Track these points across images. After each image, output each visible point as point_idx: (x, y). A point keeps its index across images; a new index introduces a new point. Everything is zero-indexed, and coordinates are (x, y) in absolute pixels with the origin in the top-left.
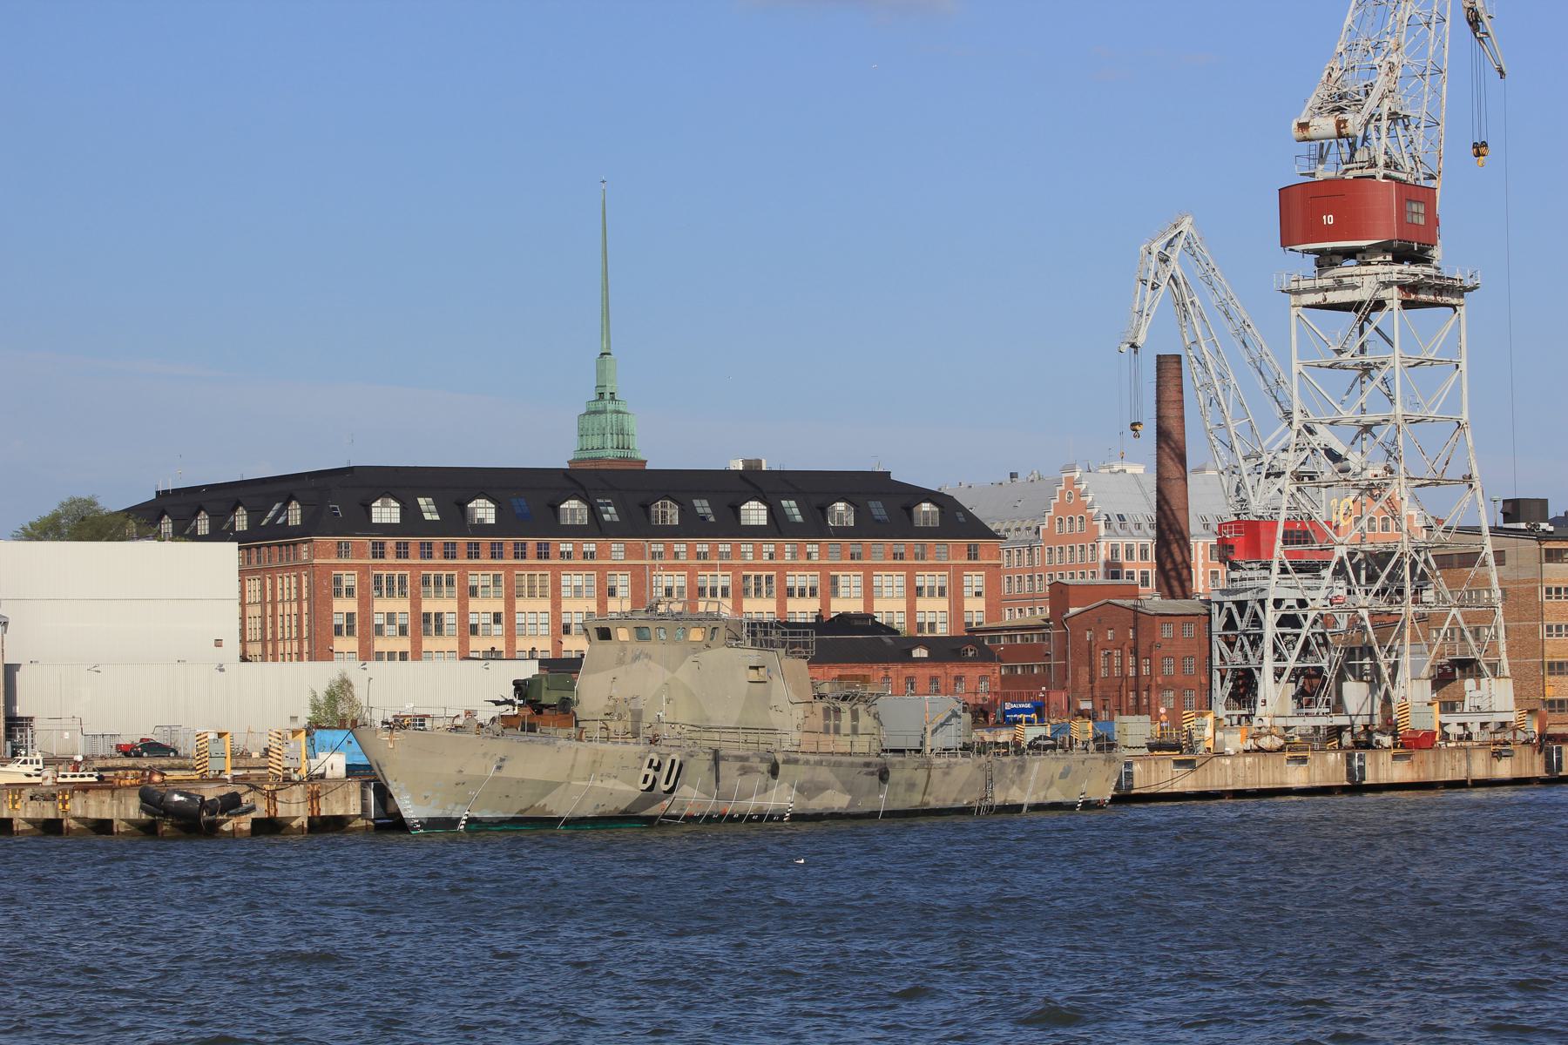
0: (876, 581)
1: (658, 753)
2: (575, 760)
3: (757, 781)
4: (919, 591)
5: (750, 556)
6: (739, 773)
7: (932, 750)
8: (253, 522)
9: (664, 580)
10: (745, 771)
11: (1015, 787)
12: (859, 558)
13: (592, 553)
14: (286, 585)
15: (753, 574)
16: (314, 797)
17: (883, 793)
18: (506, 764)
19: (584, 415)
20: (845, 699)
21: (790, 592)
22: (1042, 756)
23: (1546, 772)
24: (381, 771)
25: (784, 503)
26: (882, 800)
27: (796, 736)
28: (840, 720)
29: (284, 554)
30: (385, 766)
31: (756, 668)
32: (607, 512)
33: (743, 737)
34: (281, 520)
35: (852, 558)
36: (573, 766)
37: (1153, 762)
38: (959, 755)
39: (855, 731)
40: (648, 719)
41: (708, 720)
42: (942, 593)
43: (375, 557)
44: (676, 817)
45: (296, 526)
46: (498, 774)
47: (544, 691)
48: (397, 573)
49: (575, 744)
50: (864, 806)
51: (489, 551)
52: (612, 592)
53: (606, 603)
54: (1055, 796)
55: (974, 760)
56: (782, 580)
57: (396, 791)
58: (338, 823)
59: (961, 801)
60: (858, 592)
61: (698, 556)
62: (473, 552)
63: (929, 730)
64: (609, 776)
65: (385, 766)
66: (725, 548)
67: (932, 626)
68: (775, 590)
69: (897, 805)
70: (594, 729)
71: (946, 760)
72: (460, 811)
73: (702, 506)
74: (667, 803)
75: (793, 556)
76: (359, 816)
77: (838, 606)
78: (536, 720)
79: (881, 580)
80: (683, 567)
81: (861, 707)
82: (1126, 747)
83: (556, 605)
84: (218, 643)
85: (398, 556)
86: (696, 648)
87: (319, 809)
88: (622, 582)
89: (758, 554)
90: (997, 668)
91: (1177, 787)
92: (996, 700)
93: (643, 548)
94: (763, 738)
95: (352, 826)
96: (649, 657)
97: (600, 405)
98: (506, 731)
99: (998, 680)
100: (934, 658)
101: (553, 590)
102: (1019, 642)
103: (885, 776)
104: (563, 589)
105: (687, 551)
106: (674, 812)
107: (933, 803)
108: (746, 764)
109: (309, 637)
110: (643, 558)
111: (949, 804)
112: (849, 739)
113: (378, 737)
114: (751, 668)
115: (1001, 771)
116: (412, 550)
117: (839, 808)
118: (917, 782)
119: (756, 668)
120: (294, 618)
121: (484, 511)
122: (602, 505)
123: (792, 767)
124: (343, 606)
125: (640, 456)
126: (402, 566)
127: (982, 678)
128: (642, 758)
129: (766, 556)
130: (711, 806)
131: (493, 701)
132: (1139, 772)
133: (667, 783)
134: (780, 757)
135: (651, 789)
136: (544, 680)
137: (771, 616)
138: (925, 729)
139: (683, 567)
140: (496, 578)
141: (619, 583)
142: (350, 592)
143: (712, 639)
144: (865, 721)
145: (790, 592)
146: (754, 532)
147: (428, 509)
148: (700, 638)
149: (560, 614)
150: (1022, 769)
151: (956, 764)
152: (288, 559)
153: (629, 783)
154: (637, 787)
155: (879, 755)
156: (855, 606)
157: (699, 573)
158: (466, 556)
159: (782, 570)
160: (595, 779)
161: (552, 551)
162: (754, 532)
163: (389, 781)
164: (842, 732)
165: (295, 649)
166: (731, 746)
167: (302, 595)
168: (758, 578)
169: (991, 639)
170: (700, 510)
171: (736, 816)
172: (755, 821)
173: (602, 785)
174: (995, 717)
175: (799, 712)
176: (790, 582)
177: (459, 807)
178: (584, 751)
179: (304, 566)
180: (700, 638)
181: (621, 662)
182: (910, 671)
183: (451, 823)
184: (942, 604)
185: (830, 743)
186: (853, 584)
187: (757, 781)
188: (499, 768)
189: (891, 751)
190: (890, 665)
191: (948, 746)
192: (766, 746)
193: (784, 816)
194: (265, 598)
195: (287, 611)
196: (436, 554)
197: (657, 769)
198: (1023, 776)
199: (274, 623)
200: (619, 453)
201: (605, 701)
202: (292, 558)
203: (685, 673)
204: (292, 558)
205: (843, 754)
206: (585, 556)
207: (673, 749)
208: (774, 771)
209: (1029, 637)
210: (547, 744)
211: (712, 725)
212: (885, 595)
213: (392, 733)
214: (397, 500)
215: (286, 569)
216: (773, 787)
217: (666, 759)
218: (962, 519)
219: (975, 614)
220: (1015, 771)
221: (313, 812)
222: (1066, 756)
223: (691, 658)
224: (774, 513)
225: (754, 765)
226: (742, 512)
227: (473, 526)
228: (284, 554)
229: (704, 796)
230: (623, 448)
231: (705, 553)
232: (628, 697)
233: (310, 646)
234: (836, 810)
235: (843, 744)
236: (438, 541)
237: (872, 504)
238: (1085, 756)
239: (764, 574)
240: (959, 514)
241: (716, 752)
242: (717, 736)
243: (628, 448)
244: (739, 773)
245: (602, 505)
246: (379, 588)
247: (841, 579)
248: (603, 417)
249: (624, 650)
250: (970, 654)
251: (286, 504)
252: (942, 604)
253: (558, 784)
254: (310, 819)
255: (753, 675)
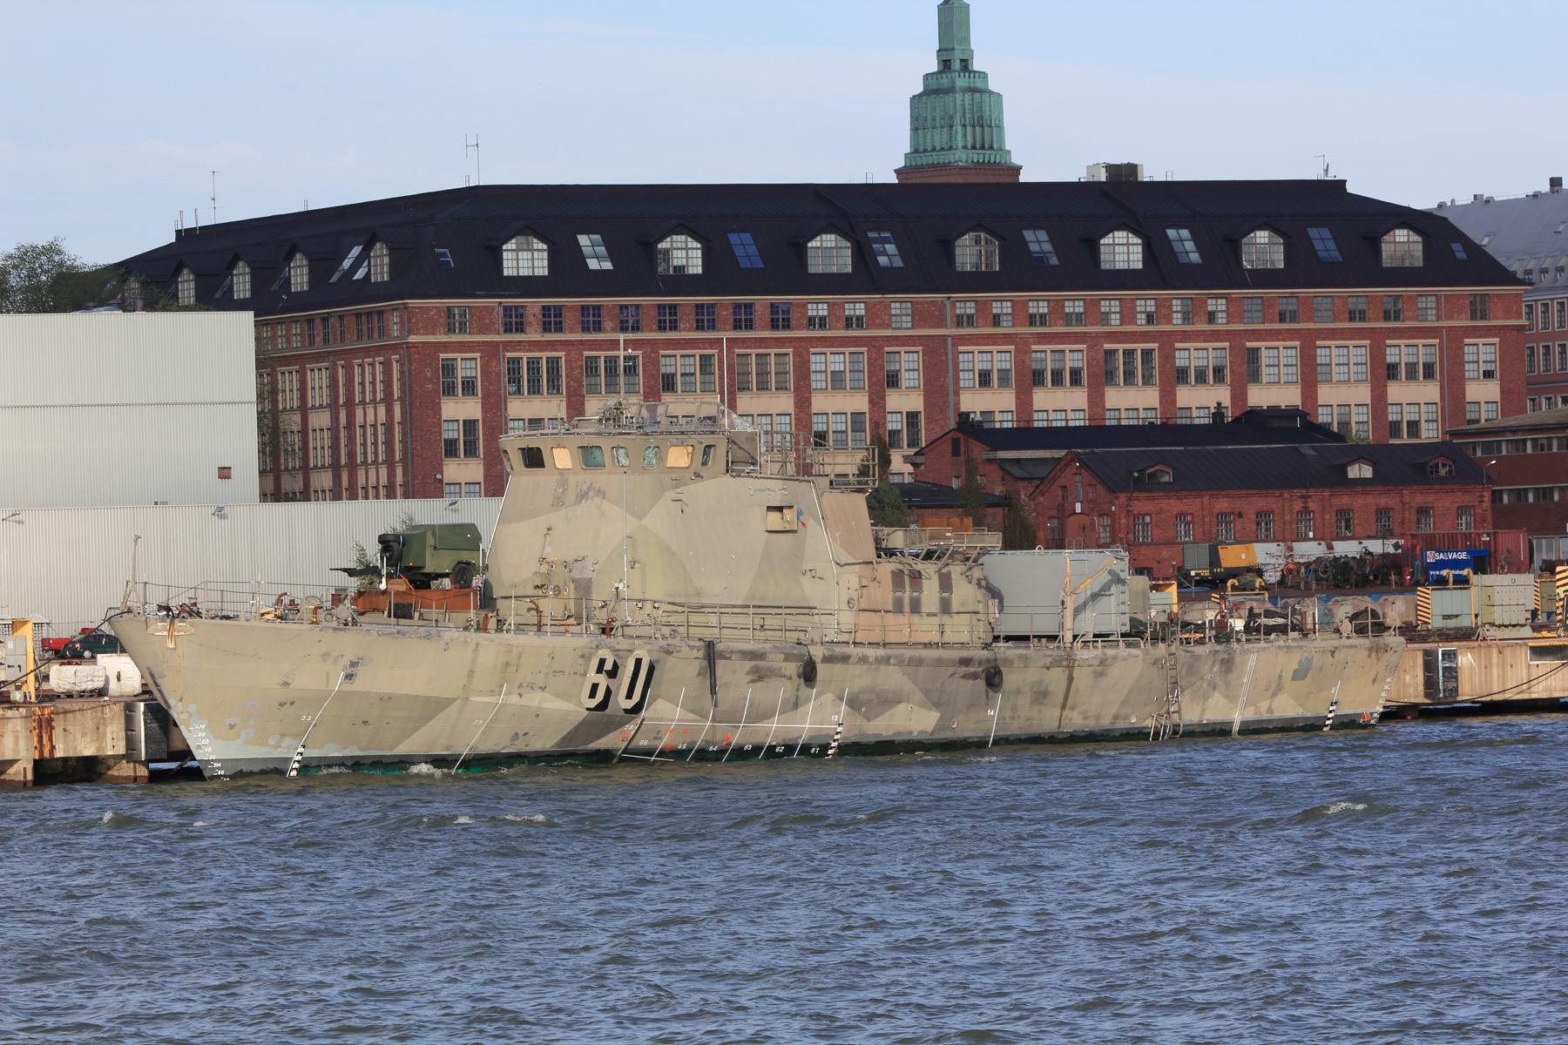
0: (1322, 356)
1: (614, 650)
2: (474, 662)
3: (781, 691)
4: (1392, 371)
5: (1115, 319)
6: (750, 678)
7: (1075, 637)
8: (318, 276)
9: (973, 359)
10: (759, 675)
11: (1217, 694)
12: (1363, 319)
13: (859, 318)
14: (368, 378)
15: (1121, 347)
16: (44, 726)
17: (994, 707)
18: (360, 671)
19: (920, 95)
20: (929, 555)
21: (1181, 375)
22: (1263, 644)
23: (1427, 695)
24: (157, 685)
25: (1171, 233)
26: (993, 718)
27: (847, 619)
28: (920, 590)
29: (365, 328)
30: (162, 677)
31: (780, 509)
32: (885, 253)
33: (758, 621)
34: (360, 274)
35: (1282, 320)
36: (471, 673)
37: (1495, 651)
38: (1121, 644)
39: (945, 608)
40: (599, 594)
41: (698, 594)
42: (1429, 373)
43: (508, 330)
44: (650, 752)
45: (383, 283)
46: (349, 687)
47: (428, 552)
48: (545, 355)
49: (473, 636)
50: (964, 727)
51: (693, 317)
52: (893, 381)
53: (883, 398)
54: (1287, 707)
55: (1147, 653)
56: (1168, 357)
57: (183, 717)
58: (88, 770)
59: (1127, 717)
60: (1293, 373)
61: (1032, 320)
62: (667, 317)
63: (1070, 605)
64: (532, 687)
65: (162, 677)
66: (1074, 306)
67: (1414, 426)
68: (1156, 372)
69: (1016, 728)
70: (511, 611)
71: (1099, 652)
72: (288, 747)
73: (1038, 241)
74: (631, 728)
75: (1186, 318)
76: (123, 757)
77: (1259, 397)
78: (416, 597)
79: (1329, 353)
80: (1007, 339)
81: (956, 570)
82: (1492, 624)
83: (803, 403)
84: (224, 473)
85: (546, 328)
86: (678, 479)
87: (53, 748)
88: (909, 364)
89: (1128, 315)
90: (1487, 497)
91: (1539, 692)
92: (1413, 548)
93: (941, 307)
94: (791, 622)
95: (114, 772)
96: (602, 493)
97: (945, 81)
98: (359, 619)
99: (1489, 513)
100: (1381, 479)
101: (797, 379)
102: (1529, 450)
103: (996, 680)
104: (813, 377)
105: (1013, 314)
106: (643, 743)
107: (1076, 721)
108: (762, 664)
109: (404, 460)
110: (942, 325)
111: (1106, 722)
112: (935, 621)
113: (150, 631)
114: (770, 508)
115: (1192, 670)
116: (568, 319)
117: (921, 732)
118: (1050, 689)
119: (780, 509)
120: (380, 430)
121: (685, 253)
122: (877, 241)
123: (838, 667)
124: (460, 410)
125: (1015, 160)
126: (552, 345)
127: (1462, 510)
128: (586, 657)
129: (1141, 319)
130: (705, 732)
131: (345, 570)
132: (1471, 667)
133: (629, 695)
134: (817, 652)
135: (603, 706)
136: (429, 534)
137: (1151, 414)
138: (1063, 603)
139: (1007, 339)
140: (706, 361)
141: (905, 366)
142: (469, 387)
143: (704, 464)
144: (964, 592)
145: (1181, 375)
146: (1122, 280)
147: (595, 255)
148: (684, 461)
149: (810, 416)
150: (1228, 664)
151: (1115, 658)
152: (370, 337)
153: (565, 697)
154: (579, 704)
155: (986, 646)
156: (1289, 397)
157: (1034, 347)
158: (655, 327)
159: (1168, 341)
160: (509, 693)
161: (794, 317)
162: (1122, 280)
163: (171, 702)
164: (924, 609)
165: (384, 479)
166: (737, 636)
167: (392, 393)
168: (1129, 354)
169: (1487, 447)
170: (1034, 247)
171: (748, 747)
172: (780, 755)
173: (521, 701)
174: (1412, 574)
175: (851, 578)
176: (1181, 360)
177: (287, 742)
178: (491, 647)
179: (395, 348)
180: (684, 461)
181: (559, 502)
182: (1344, 500)
183: (275, 771)
184: (1429, 392)
185: (901, 627)
186: (1283, 361)
187: (781, 691)
188: (349, 677)
189: (1008, 639)
190: (1311, 492)
191: (1103, 629)
192: (795, 635)
193: (828, 746)
194: (337, 398)
195: (370, 419)
196: (608, 324)
197: (613, 674)
198: (1231, 677)
199: (351, 439)
200: (977, 156)
201: (534, 566)
202: (376, 334)
203: (658, 520)
204: (376, 334)
205: (927, 645)
206: (848, 323)
207: (637, 642)
208: (809, 674)
209: (1545, 442)
210: (428, 637)
211: (705, 601)
212: (1335, 378)
213: (172, 622)
214: (543, 239)
215: (367, 352)
216: (808, 701)
217: (627, 658)
218: (1461, 255)
219: (1484, 407)
220: (1216, 668)
221: (41, 752)
222: (1302, 643)
223: (670, 495)
224: (1155, 250)
225: (776, 665)
226: (1102, 249)
227: (666, 278)
228: (365, 328)
229: (692, 716)
230: (983, 147)
231: (1042, 316)
232: (570, 559)
233: (405, 474)
234: (915, 735)
235: (926, 629)
236: (761, 301)
237: (1313, 232)
238: (1336, 643)
239: (1139, 347)
240: (1456, 247)
241: (710, 646)
242: (713, 620)
243: (991, 148)
244: (750, 678)
245: (877, 241)
246: (515, 378)
247: (1264, 353)
248: (948, 98)
249: (564, 483)
250: (1443, 472)
251: (367, 248)
252: (1429, 392)
253: (448, 702)
254: (37, 764)
255: (774, 520)
